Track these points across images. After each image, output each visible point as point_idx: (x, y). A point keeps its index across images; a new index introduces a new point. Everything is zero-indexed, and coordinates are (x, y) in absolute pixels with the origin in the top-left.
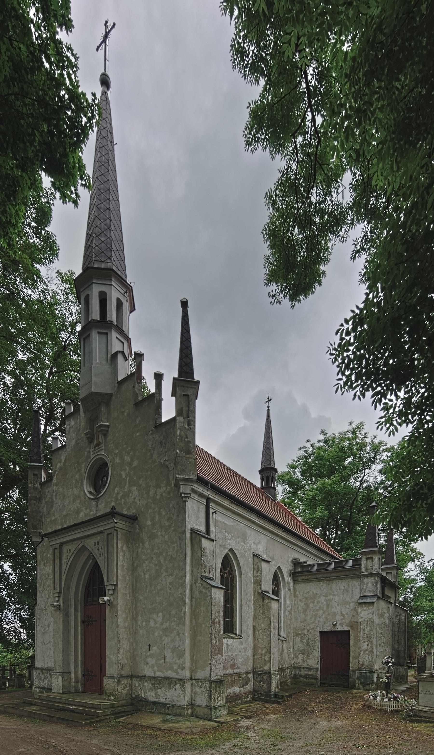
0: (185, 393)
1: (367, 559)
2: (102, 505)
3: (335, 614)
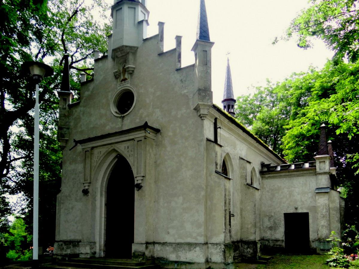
0: (204, 50)
1: (320, 162)
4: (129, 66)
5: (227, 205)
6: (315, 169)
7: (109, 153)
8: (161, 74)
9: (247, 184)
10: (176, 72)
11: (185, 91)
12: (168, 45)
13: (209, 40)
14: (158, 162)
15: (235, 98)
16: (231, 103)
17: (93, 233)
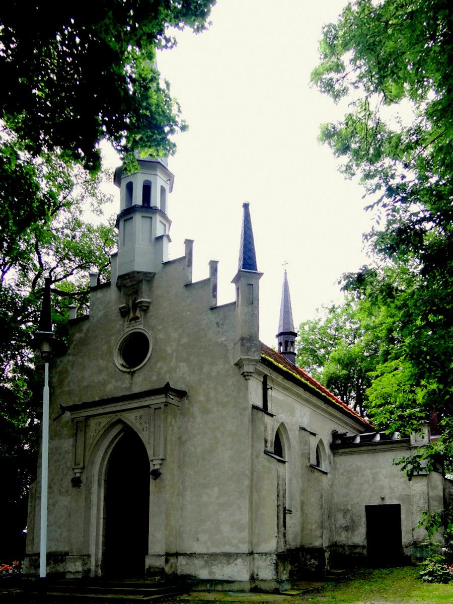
2: (139, 378)
3: (382, 488)
4: (142, 300)
5: (281, 498)
6: (409, 441)
7: (112, 425)
8: (188, 313)
9: (311, 466)
10: (210, 311)
11: (223, 339)
12: (199, 273)
13: (256, 270)
14: (184, 439)
15: (296, 332)
16: (290, 338)
17: (86, 543)
